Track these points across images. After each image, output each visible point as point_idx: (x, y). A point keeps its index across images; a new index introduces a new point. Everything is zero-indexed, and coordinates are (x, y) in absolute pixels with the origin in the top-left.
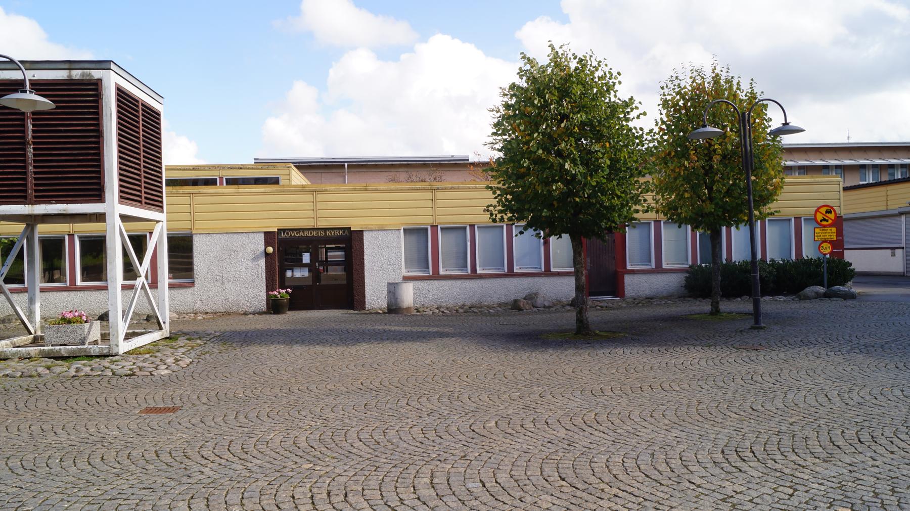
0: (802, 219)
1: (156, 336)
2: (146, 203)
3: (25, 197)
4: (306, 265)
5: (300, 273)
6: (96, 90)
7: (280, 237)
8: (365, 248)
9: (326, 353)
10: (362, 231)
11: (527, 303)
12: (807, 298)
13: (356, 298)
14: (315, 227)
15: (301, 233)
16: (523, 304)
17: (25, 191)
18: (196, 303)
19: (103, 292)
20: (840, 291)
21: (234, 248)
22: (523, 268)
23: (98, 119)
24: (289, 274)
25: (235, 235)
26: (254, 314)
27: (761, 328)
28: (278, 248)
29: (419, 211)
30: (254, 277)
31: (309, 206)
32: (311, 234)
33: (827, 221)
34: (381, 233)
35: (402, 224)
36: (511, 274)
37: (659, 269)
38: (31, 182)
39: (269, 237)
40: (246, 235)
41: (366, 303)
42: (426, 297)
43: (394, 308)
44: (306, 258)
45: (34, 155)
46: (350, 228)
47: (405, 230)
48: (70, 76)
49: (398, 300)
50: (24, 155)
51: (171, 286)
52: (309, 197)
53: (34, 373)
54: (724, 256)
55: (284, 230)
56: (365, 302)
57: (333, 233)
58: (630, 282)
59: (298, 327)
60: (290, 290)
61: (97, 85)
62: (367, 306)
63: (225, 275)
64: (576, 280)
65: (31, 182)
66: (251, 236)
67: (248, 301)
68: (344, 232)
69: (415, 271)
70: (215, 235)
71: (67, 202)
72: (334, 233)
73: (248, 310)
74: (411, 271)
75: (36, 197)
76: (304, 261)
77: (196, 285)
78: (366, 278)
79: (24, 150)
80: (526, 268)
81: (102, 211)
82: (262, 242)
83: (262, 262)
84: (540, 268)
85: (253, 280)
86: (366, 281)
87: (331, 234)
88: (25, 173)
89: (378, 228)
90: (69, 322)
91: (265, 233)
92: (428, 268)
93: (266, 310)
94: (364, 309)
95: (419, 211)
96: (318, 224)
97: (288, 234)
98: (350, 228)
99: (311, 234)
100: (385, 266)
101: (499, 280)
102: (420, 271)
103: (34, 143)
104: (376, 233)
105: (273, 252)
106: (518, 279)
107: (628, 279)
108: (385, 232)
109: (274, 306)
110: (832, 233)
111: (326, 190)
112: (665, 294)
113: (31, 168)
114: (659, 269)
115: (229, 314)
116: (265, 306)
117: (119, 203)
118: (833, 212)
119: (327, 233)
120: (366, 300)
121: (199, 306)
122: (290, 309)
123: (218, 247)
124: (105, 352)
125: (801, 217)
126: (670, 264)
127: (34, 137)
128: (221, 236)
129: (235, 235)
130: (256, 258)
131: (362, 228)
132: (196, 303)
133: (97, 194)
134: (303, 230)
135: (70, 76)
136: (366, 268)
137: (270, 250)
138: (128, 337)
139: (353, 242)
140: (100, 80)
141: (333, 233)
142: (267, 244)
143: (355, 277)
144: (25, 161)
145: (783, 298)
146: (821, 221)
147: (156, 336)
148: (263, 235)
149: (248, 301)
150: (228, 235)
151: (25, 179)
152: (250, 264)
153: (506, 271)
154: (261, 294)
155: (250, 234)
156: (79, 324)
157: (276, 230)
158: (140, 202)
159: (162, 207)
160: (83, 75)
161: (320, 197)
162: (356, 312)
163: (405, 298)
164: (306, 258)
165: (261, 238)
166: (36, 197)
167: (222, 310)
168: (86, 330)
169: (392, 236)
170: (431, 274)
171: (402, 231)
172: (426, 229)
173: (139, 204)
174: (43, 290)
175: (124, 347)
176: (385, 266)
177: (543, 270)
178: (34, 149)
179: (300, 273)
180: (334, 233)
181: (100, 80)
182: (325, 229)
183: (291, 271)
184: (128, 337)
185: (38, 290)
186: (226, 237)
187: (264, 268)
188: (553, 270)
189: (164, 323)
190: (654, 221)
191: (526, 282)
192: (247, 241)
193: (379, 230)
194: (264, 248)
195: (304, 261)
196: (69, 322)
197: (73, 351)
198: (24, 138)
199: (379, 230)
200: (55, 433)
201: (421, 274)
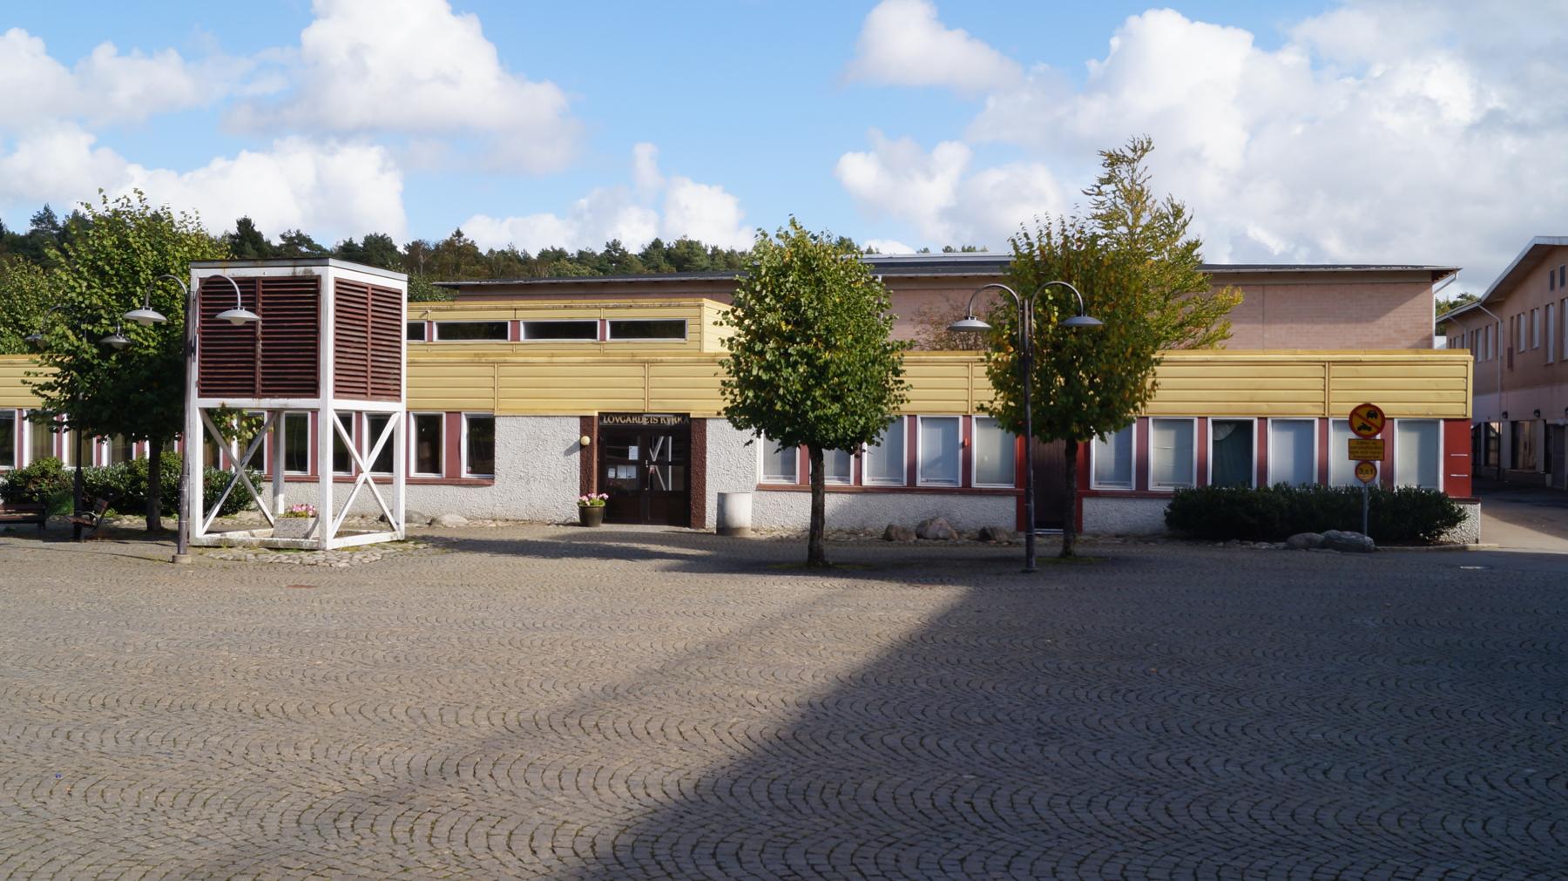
0: (1396, 421)
1: (385, 537)
2: (372, 394)
3: (253, 391)
4: (633, 463)
5: (625, 474)
6: (316, 286)
9: (536, 564)
10: (705, 419)
12: (1292, 547)
15: (629, 419)
16: (896, 533)
17: (254, 385)
18: (495, 506)
19: (313, 485)
20: (1339, 538)
22: (932, 481)
23: (316, 315)
24: (611, 474)
25: (545, 419)
27: (1033, 571)
31: (639, 381)
33: (1369, 429)
36: (912, 488)
37: (1142, 492)
38: (259, 377)
39: (586, 423)
42: (787, 516)
44: (634, 452)
45: (263, 350)
46: (689, 414)
48: (294, 273)
49: (727, 517)
50: (254, 351)
51: (336, 480)
52: (639, 370)
53: (243, 558)
55: (607, 415)
56: (704, 518)
58: (1092, 510)
59: (545, 540)
61: (316, 282)
62: (707, 523)
63: (531, 472)
64: (813, 496)
65: (259, 377)
66: (564, 421)
71: (288, 397)
73: (558, 520)
75: (263, 391)
76: (630, 458)
77: (496, 482)
79: (254, 345)
80: (937, 481)
81: (316, 407)
82: (578, 430)
83: (577, 456)
84: (957, 482)
88: (254, 368)
90: (297, 515)
91: (582, 418)
98: (689, 414)
100: (734, 468)
101: (892, 497)
102: (785, 478)
103: (263, 339)
106: (919, 496)
107: (1088, 505)
109: (586, 516)
110: (1376, 448)
111: (661, 362)
112: (1147, 531)
113: (259, 364)
114: (1142, 492)
117: (335, 397)
118: (1379, 416)
120: (707, 515)
121: (499, 511)
124: (315, 546)
125: (1393, 419)
126: (1164, 485)
127: (263, 333)
128: (527, 419)
130: (569, 452)
132: (495, 506)
133: (313, 389)
135: (294, 273)
137: (586, 440)
138: (339, 535)
139: (693, 433)
140: (319, 276)
142: (584, 432)
143: (694, 482)
144: (254, 357)
145: (1265, 545)
146: (1360, 429)
147: (385, 537)
148: (578, 420)
151: (254, 374)
152: (561, 457)
153: (905, 484)
156: (304, 519)
157: (596, 414)
158: (366, 394)
159: (399, 396)
160: (305, 272)
161: (654, 370)
164: (634, 452)
165: (576, 425)
166: (263, 391)
168: (310, 526)
173: (364, 396)
174: (289, 480)
175: (332, 543)
176: (734, 468)
177: (960, 485)
178: (263, 345)
179: (625, 474)
181: (319, 276)
184: (339, 535)
185: (282, 480)
187: (579, 464)
188: (975, 485)
189: (398, 524)
191: (932, 501)
195: (630, 458)
196: (297, 515)
197: (288, 543)
198: (254, 333)
200: (554, 852)
201: (784, 482)
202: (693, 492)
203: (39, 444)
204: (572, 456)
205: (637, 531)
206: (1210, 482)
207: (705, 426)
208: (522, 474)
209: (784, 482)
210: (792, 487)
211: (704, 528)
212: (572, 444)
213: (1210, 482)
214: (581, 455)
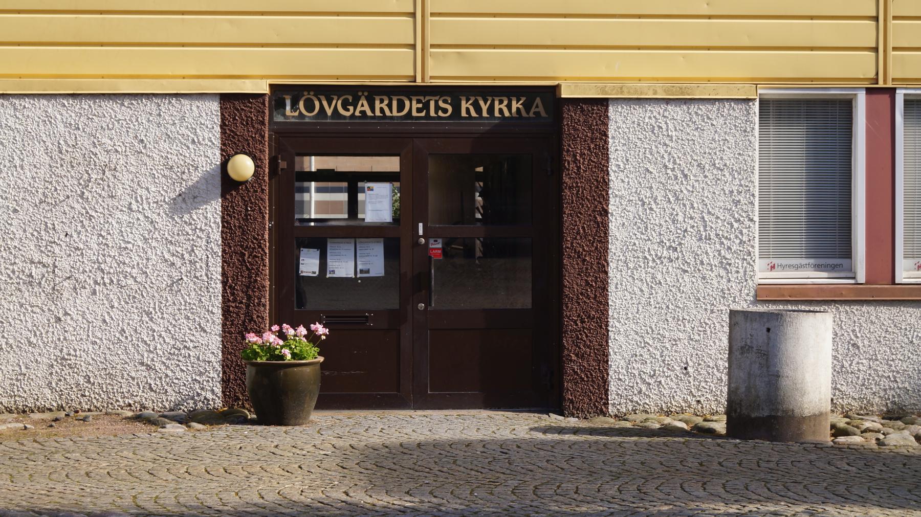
7: (279, 119)
8: (612, 167)
10: (603, 103)
11: (47, 272)
13: (573, 365)
14: (419, 82)
21: (103, 158)
26: (186, 420)
28: (273, 162)
29: (825, 32)
30: (175, 275)
32: (401, 107)
34: (677, 112)
35: (756, 82)
40: (150, 106)
41: (612, 388)
43: (766, 413)
46: (555, 89)
47: (762, 102)
49: (785, 383)
54: (314, 163)
56: (605, 382)
57: (485, 108)
60: (321, 330)
63: (64, 264)
66: (171, 109)
67: (149, 368)
68: (527, 106)
69: (797, 268)
70: (27, 102)
72: (491, 110)
73: (153, 403)
74: (784, 267)
78: (611, 288)
82: (212, 134)
83: (213, 210)
85: (174, 284)
86: (616, 298)
87: (478, 109)
89: (666, 91)
91: (225, 99)
92: (847, 253)
93: (219, 403)
94: (600, 405)
95: (825, 32)
96: (430, 72)
97: (310, 107)
98: (555, 89)
99: (401, 107)
100: (690, 242)
102: (818, 268)
104: (657, 109)
105: (256, 174)
108: (693, 108)
115: (79, 416)
116: (218, 390)
119: (464, 105)
122: (323, 404)
123: (39, 149)
128: (51, 107)
129: (108, 106)
131: (603, 91)
134: (373, 92)
136: (615, 248)
141: (485, 108)
143: (572, 281)
148: (215, 106)
149: (149, 368)
150: (76, 104)
152: (162, 222)
154: (202, 339)
155: (164, 104)
157: (266, 90)
162: (572, 422)
163: (808, 378)
167: (49, 398)
169: (192, 108)
170: (861, 277)
171: (756, 107)
172: (847, 105)
180: (491, 110)
182: (454, 93)
183: (316, 253)
186: (72, 111)
187: (217, 236)
190: (869, 91)
192: (154, 129)
193: (668, 101)
194: (217, 159)
199: (668, 101)
201: (821, 278)
202: (571, 312)
203: (508, 443)
204: (196, 215)
205: (424, 434)
206: (462, 248)
207: (604, 120)
208: (37, 272)
209: (821, 278)
210: (835, 290)
211: (604, 414)
212: (195, 177)
213: (462, 248)
214: (224, 208)
